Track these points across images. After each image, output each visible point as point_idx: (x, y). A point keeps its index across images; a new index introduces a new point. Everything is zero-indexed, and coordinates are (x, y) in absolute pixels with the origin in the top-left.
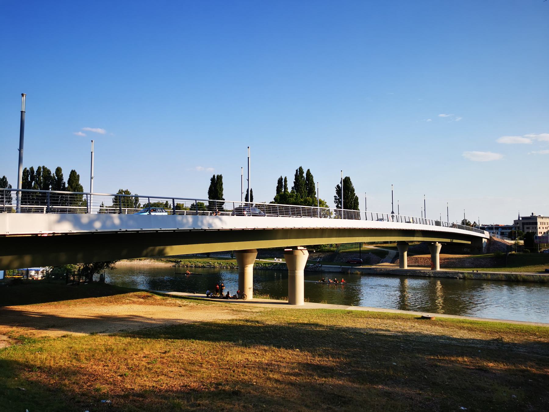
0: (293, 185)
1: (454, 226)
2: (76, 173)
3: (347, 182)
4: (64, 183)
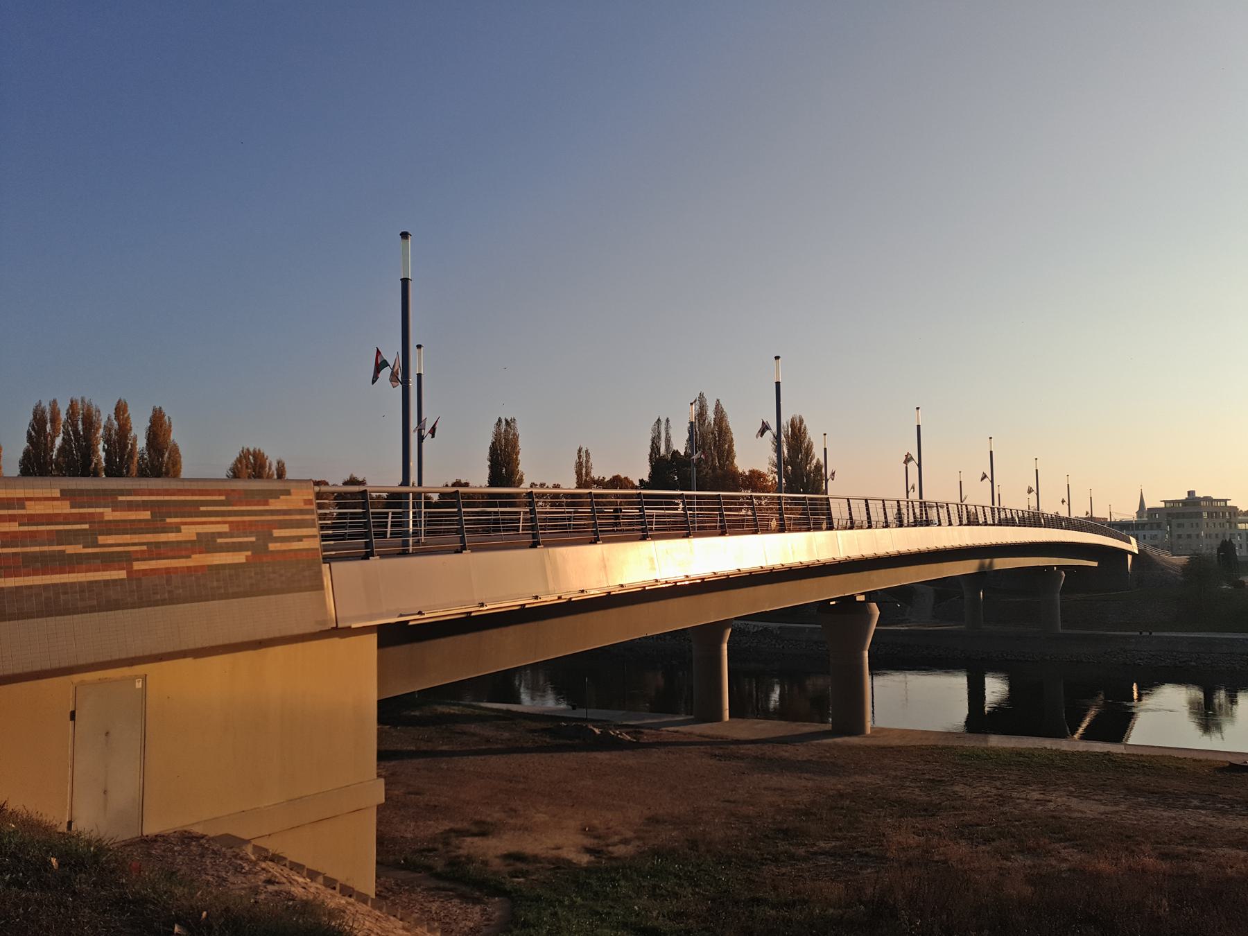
3: (55, 401)
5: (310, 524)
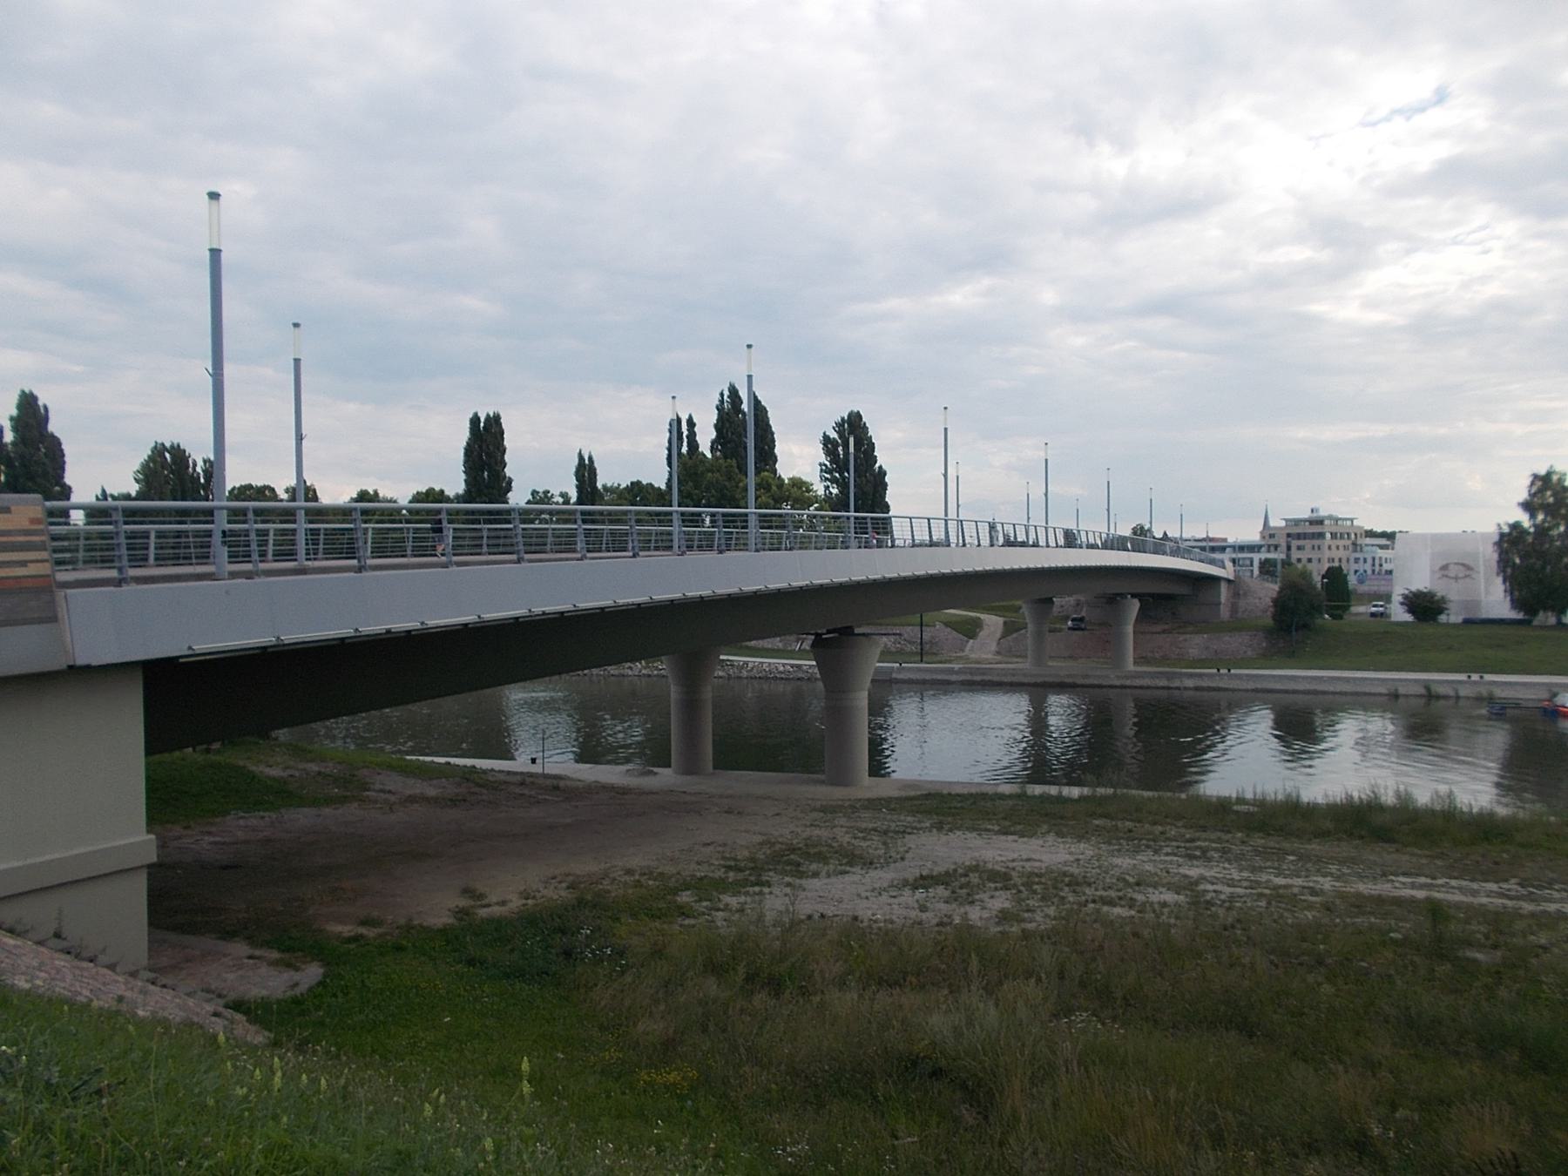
0: (714, 435)
3: (853, 426)
5: (40, 547)
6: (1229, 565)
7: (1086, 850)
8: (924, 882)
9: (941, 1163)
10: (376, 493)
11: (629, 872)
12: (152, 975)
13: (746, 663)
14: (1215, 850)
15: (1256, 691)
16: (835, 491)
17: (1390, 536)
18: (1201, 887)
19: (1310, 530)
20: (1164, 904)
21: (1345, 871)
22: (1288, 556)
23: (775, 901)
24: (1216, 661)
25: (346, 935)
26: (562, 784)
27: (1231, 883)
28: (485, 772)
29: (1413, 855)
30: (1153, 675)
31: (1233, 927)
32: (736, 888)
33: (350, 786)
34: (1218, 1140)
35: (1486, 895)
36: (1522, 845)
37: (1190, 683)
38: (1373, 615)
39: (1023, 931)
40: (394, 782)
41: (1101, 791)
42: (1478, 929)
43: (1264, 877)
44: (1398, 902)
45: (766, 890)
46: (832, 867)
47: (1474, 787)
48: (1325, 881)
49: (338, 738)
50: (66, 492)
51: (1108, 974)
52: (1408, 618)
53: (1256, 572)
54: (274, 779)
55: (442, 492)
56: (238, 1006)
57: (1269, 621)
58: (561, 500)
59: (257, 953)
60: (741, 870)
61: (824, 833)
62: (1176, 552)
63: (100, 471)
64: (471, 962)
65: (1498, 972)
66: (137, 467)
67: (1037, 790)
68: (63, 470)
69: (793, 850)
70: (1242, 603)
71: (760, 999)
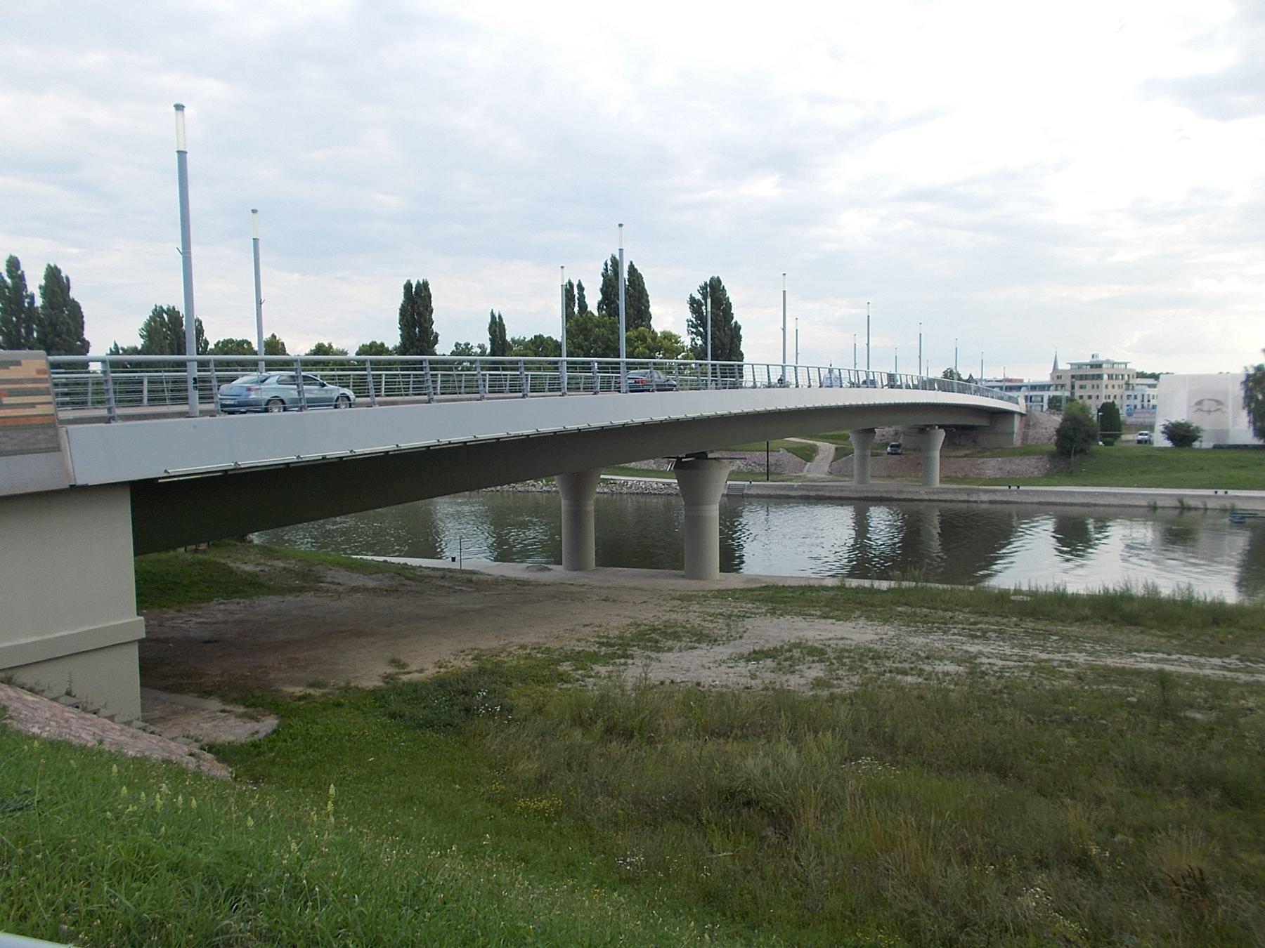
0: (600, 297)
1: (927, 384)
2: (59, 271)
3: (714, 290)
4: (32, 297)
6: (1022, 401)
7: (889, 631)
8: (757, 655)
9: (748, 872)
10: (330, 346)
11: (523, 647)
12: (143, 724)
13: (627, 482)
14: (994, 631)
15: (1040, 503)
16: (699, 342)
17: (1155, 377)
18: (978, 661)
19: (1091, 373)
20: (947, 674)
21: (1098, 648)
22: (1072, 394)
23: (632, 673)
24: (1009, 480)
25: (298, 694)
26: (474, 578)
27: (1004, 657)
28: (414, 568)
29: (1154, 635)
30: (954, 491)
31: (1001, 692)
32: (607, 659)
33: (307, 579)
34: (966, 857)
35: (1211, 668)
36: (1245, 628)
37: (985, 497)
38: (1139, 442)
39: (831, 694)
40: (343, 576)
41: (905, 584)
42: (1200, 694)
43: (1031, 653)
44: (1138, 673)
45: (630, 661)
46: (683, 644)
47: (1218, 584)
48: (1077, 656)
49: (301, 539)
50: (85, 347)
51: (887, 728)
52: (1168, 444)
53: (1046, 407)
54: (249, 573)
55: (383, 345)
56: (211, 748)
57: (1053, 448)
58: (479, 351)
59: (228, 708)
60: (612, 646)
61: (679, 617)
62: (978, 391)
63: (111, 330)
64: (393, 716)
65: (1212, 729)
66: (142, 325)
67: (854, 583)
68: (83, 328)
69: (654, 630)
70: (1031, 432)
71: (615, 746)
